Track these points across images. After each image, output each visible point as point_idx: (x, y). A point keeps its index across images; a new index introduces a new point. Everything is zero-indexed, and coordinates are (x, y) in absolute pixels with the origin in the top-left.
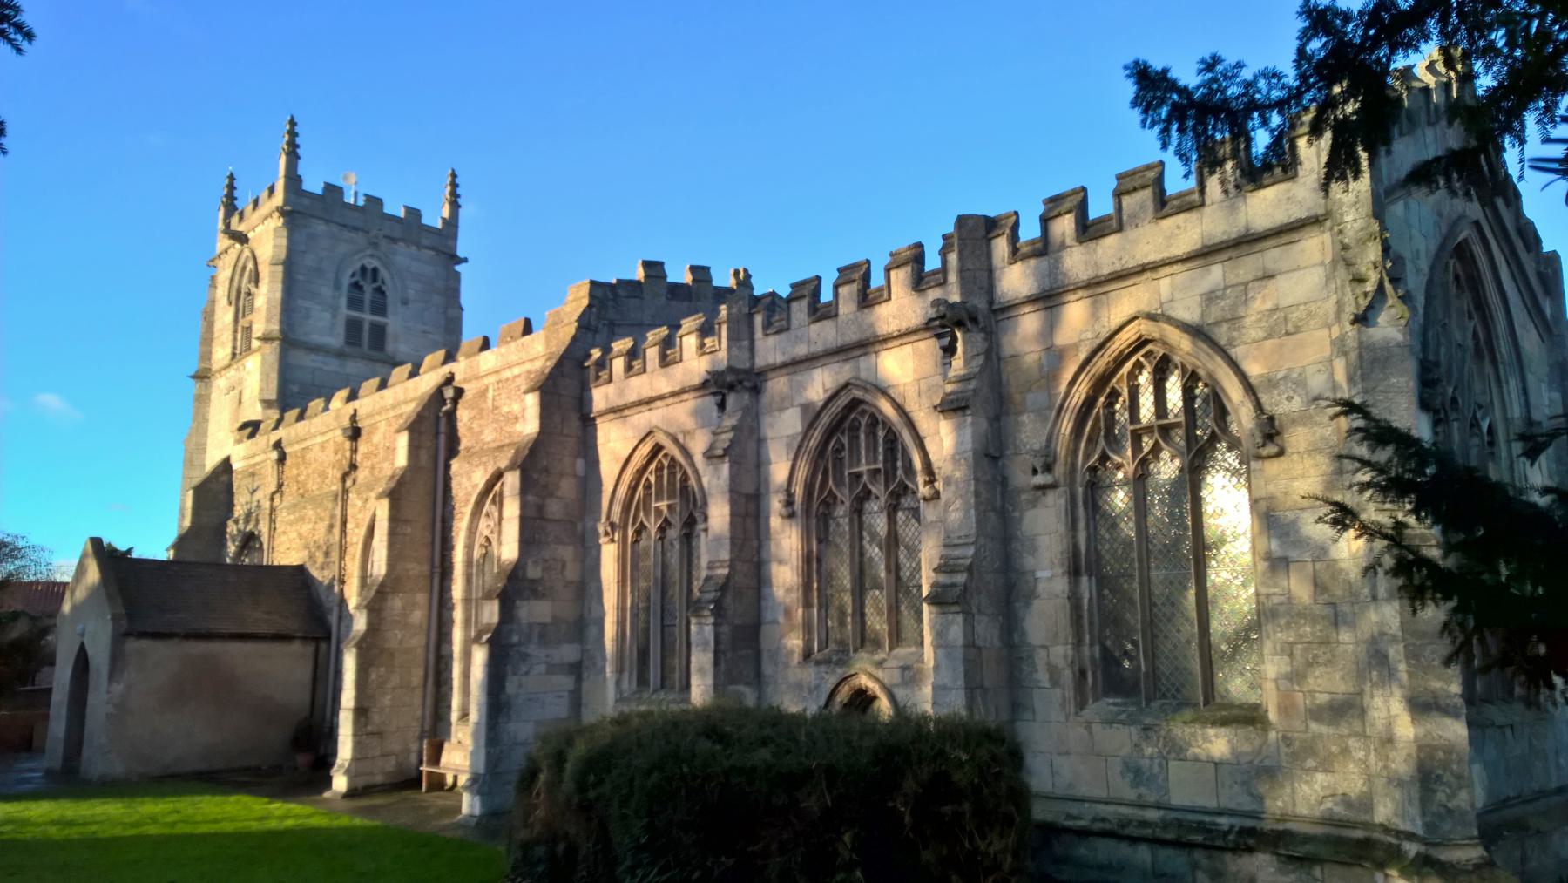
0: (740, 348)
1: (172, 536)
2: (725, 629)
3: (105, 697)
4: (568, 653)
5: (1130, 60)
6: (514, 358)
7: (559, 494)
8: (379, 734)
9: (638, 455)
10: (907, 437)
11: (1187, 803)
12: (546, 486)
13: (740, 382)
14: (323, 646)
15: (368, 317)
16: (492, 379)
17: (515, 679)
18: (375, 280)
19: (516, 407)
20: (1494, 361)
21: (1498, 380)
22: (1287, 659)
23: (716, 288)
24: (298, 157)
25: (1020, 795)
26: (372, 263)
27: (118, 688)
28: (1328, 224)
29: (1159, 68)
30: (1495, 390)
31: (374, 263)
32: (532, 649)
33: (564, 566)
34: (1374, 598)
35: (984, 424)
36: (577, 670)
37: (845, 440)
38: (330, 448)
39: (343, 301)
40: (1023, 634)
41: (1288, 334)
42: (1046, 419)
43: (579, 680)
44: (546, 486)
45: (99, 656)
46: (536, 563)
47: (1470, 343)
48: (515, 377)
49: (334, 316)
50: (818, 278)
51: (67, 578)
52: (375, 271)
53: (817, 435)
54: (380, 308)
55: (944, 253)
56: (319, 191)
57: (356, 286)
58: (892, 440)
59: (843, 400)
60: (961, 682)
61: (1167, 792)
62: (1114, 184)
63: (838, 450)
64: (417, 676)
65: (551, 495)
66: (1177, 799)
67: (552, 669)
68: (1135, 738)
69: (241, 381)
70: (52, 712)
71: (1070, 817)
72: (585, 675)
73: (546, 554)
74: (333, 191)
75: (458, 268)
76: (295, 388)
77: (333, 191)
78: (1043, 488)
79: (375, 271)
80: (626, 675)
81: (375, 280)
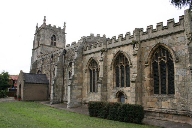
2: (102, 84)
4: (81, 87)
5: (21, 70)
10: (128, 59)
22: (178, 89)
26: (54, 34)
35: (139, 58)
36: (82, 89)
37: (119, 58)
38: (49, 59)
43: (82, 91)
50: (115, 36)
52: (55, 35)
54: (55, 40)
55: (133, 33)
56: (48, 25)
57: (52, 37)
59: (119, 53)
60: (135, 92)
62: (167, 22)
63: (119, 60)
64: (61, 89)
67: (78, 89)
74: (50, 25)
77: (50, 25)
78: (147, 66)
79: (55, 35)
80: (88, 90)
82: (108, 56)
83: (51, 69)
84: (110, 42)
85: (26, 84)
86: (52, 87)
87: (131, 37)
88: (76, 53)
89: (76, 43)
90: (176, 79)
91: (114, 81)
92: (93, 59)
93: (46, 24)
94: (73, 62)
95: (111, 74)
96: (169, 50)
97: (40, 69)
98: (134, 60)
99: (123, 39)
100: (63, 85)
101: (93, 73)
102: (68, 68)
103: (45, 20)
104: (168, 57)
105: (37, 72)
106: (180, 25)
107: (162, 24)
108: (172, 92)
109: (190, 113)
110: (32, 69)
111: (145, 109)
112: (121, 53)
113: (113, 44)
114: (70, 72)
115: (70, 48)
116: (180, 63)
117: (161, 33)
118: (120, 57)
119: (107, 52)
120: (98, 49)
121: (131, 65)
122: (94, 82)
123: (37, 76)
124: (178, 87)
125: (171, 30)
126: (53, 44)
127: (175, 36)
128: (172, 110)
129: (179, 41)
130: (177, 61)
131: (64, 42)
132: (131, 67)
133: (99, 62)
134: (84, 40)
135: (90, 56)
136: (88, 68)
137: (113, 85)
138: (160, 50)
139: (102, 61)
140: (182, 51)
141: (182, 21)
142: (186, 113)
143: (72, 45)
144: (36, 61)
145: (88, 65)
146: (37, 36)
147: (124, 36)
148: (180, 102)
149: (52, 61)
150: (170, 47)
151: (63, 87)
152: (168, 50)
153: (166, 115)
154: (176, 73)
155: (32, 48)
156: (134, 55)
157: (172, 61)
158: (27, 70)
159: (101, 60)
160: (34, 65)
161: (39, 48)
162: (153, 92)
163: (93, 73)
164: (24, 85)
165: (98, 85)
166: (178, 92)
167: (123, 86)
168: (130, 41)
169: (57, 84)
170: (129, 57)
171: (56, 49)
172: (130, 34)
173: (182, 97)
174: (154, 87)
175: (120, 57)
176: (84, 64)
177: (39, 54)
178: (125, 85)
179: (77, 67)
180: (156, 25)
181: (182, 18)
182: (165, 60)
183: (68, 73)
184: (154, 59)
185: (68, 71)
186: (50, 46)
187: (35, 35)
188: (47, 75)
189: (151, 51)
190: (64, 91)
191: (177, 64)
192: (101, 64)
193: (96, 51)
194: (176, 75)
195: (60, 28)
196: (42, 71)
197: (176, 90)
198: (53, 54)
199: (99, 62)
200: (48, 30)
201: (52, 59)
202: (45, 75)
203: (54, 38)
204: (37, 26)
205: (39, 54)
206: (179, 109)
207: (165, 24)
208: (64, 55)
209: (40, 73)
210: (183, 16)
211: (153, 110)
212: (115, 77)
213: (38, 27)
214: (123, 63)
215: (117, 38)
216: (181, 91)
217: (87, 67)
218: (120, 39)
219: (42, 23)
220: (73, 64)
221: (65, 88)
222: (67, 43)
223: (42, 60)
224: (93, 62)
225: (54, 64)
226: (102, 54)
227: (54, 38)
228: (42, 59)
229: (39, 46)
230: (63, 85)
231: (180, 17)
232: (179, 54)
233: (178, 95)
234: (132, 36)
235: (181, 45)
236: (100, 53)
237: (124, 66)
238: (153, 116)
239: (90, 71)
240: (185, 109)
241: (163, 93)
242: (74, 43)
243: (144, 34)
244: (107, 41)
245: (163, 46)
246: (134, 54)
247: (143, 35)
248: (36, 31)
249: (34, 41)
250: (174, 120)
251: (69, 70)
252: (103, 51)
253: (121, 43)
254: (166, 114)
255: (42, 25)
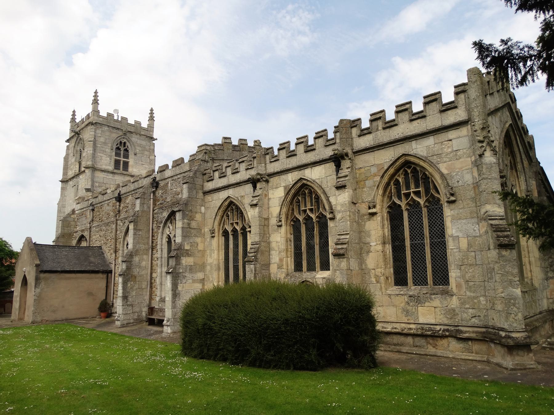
0: (261, 167)
1: (54, 238)
3: (34, 293)
4: (200, 275)
6: (178, 172)
7: (195, 219)
8: (132, 305)
9: (224, 205)
10: (323, 197)
11: (425, 322)
12: (191, 216)
13: (262, 178)
14: (110, 274)
15: (122, 159)
16: (170, 179)
17: (181, 285)
18: (124, 146)
19: (179, 190)
20: (516, 171)
21: (518, 177)
23: (249, 147)
24: (98, 104)
25: (372, 321)
27: (38, 290)
28: (470, 122)
29: (488, 43)
30: (517, 180)
31: (125, 140)
32: (187, 274)
33: (198, 245)
34: (489, 249)
37: (300, 198)
38: (111, 204)
39: (114, 153)
40: (366, 265)
41: (457, 159)
42: (373, 190)
44: (191, 216)
45: (31, 280)
46: (188, 244)
47: (509, 164)
48: (179, 178)
49: (111, 159)
51: (19, 251)
53: (290, 197)
54: (126, 156)
55: (335, 132)
57: (118, 149)
58: (318, 198)
59: (299, 185)
61: (418, 318)
62: (395, 109)
65: (193, 220)
66: (421, 320)
67: (194, 281)
68: (406, 300)
69: (78, 183)
70: (14, 299)
71: (383, 327)
72: (206, 283)
73: (191, 241)
75: (153, 142)
76: (97, 185)
79: (125, 143)
81: (124, 146)
82: (271, 192)
83: (116, 231)
84: (212, 178)
85: (42, 275)
86: (120, 280)
87: (329, 143)
88: (185, 186)
89: (186, 160)
90: (451, 245)
91: (287, 257)
92: (231, 203)
93: (98, 112)
94: (179, 211)
95: (279, 239)
96: (430, 174)
97: (86, 234)
98: (340, 200)
99: (309, 149)
100: (151, 274)
101: (231, 238)
102: (164, 227)
103: (96, 102)
104: (427, 191)
105: (74, 243)
106: (456, 107)
107: (411, 107)
108: (442, 277)
109: (495, 334)
110: (60, 232)
111: (379, 327)
112: (304, 185)
113: (284, 163)
114: (169, 238)
115: (168, 173)
116: (459, 204)
117: (405, 128)
118: (410, 174)
119: (267, 181)
120: (243, 175)
121: (332, 213)
122: (236, 260)
123: (77, 251)
124: (460, 267)
125: (434, 120)
126: (121, 165)
127: (443, 136)
128: (446, 327)
129: (455, 149)
130: (453, 198)
131: (153, 162)
132: (332, 219)
133: (248, 208)
134: (205, 153)
135: (223, 195)
136: (220, 225)
137: (285, 267)
138: (406, 174)
139: (256, 205)
140: (465, 172)
141: (462, 96)
142: (484, 332)
143: (173, 167)
144: (73, 211)
145: (218, 218)
146: (73, 144)
147: (311, 142)
148: (467, 306)
149: (119, 211)
150: (431, 164)
151: (151, 278)
152: (427, 173)
153: (431, 341)
154: (451, 229)
155: (61, 178)
156: (252, 206)
157: (439, 200)
158: (47, 236)
159: (255, 202)
160: (66, 222)
161: (81, 177)
162: (393, 282)
163: (231, 238)
164: (37, 279)
165: (247, 269)
166: (458, 279)
167: (311, 268)
168: (329, 152)
169: (136, 271)
170: (324, 193)
171: (128, 178)
172: (326, 135)
173: (470, 291)
174: (394, 269)
175: (302, 192)
176: (207, 216)
177: (82, 193)
178: (318, 264)
179: (189, 224)
180: (369, 117)
181: (461, 89)
182: (420, 197)
183: (165, 240)
184: (390, 198)
185: (165, 236)
186: (113, 173)
187: (68, 141)
188: (104, 247)
189: (382, 177)
190: (154, 289)
191: (453, 206)
192: (251, 214)
193: (238, 181)
194: (452, 236)
195: (138, 123)
196: (90, 237)
197: (454, 274)
198: (122, 192)
199: (248, 208)
200: (106, 128)
201: (120, 206)
202: (100, 247)
203: (122, 150)
204: (73, 119)
205: (82, 193)
206: (464, 323)
207: (418, 107)
208: (154, 193)
209: (84, 244)
210: (464, 84)
211: (396, 328)
212: (289, 247)
213: (78, 119)
214: (311, 210)
215: (293, 147)
216: (468, 276)
217: (216, 223)
218: (301, 148)
219: (89, 109)
220: (178, 216)
221: (158, 281)
222: (159, 163)
223: (91, 208)
224: (232, 208)
225: (126, 218)
226: (255, 187)
227: (122, 150)
228: (91, 205)
229: (81, 173)
230: (151, 274)
231: (455, 87)
232: (453, 183)
233: (459, 286)
234: (332, 139)
235: (460, 158)
236: (249, 187)
237: (313, 216)
238: (395, 345)
239: (225, 234)
240: (481, 324)
241: (420, 280)
242: (178, 163)
243: (364, 133)
244: (268, 154)
245: (414, 164)
246: (338, 185)
247: (359, 136)
248: (72, 131)
249: (66, 159)
250: (451, 349)
251: (167, 231)
252: (258, 180)
253: (303, 158)
254: (430, 335)
255: (88, 115)
